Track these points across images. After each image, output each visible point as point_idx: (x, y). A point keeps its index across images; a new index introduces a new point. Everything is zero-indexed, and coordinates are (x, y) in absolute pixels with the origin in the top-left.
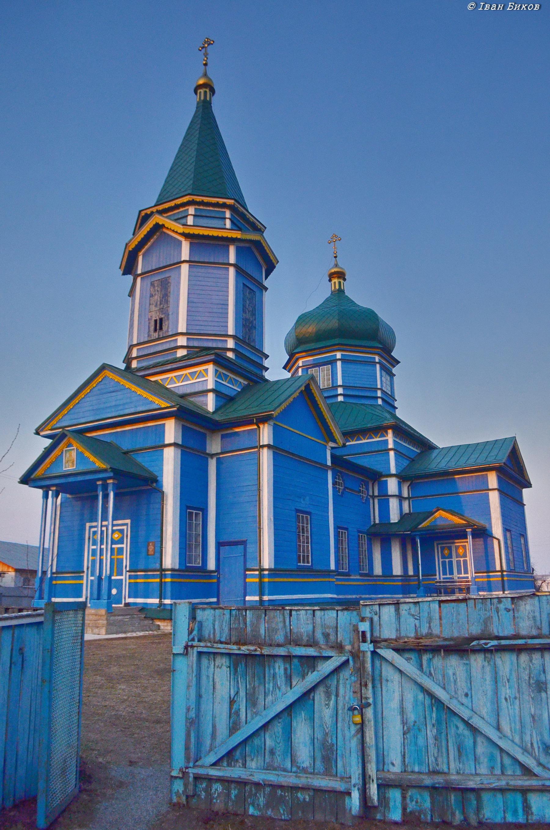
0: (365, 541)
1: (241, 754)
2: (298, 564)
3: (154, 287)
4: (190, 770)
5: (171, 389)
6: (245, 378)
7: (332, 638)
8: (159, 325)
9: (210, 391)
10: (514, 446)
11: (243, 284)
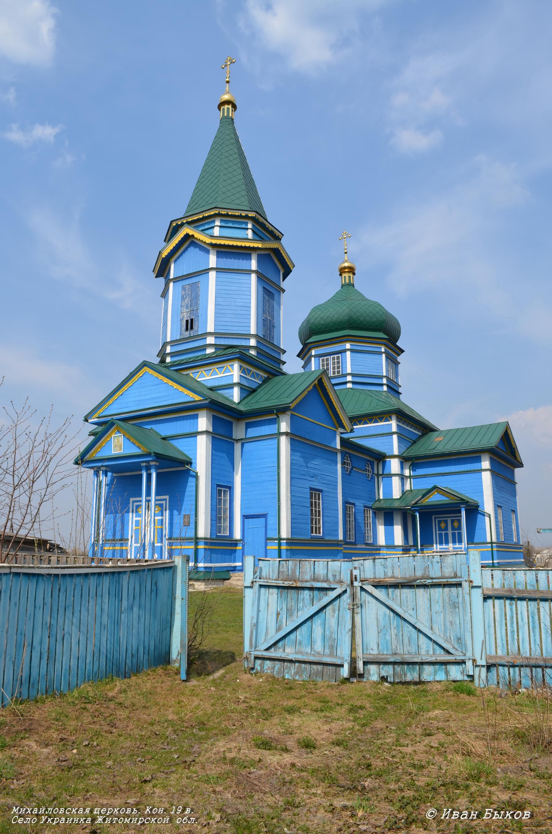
0: (370, 514)
1: (282, 644)
2: (218, 534)
3: (185, 291)
4: (252, 653)
5: (201, 382)
6: (265, 371)
7: (338, 578)
8: (190, 325)
9: (235, 384)
10: (506, 429)
11: (264, 287)
